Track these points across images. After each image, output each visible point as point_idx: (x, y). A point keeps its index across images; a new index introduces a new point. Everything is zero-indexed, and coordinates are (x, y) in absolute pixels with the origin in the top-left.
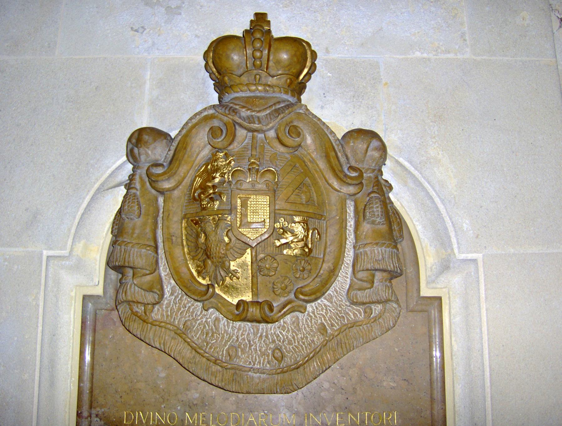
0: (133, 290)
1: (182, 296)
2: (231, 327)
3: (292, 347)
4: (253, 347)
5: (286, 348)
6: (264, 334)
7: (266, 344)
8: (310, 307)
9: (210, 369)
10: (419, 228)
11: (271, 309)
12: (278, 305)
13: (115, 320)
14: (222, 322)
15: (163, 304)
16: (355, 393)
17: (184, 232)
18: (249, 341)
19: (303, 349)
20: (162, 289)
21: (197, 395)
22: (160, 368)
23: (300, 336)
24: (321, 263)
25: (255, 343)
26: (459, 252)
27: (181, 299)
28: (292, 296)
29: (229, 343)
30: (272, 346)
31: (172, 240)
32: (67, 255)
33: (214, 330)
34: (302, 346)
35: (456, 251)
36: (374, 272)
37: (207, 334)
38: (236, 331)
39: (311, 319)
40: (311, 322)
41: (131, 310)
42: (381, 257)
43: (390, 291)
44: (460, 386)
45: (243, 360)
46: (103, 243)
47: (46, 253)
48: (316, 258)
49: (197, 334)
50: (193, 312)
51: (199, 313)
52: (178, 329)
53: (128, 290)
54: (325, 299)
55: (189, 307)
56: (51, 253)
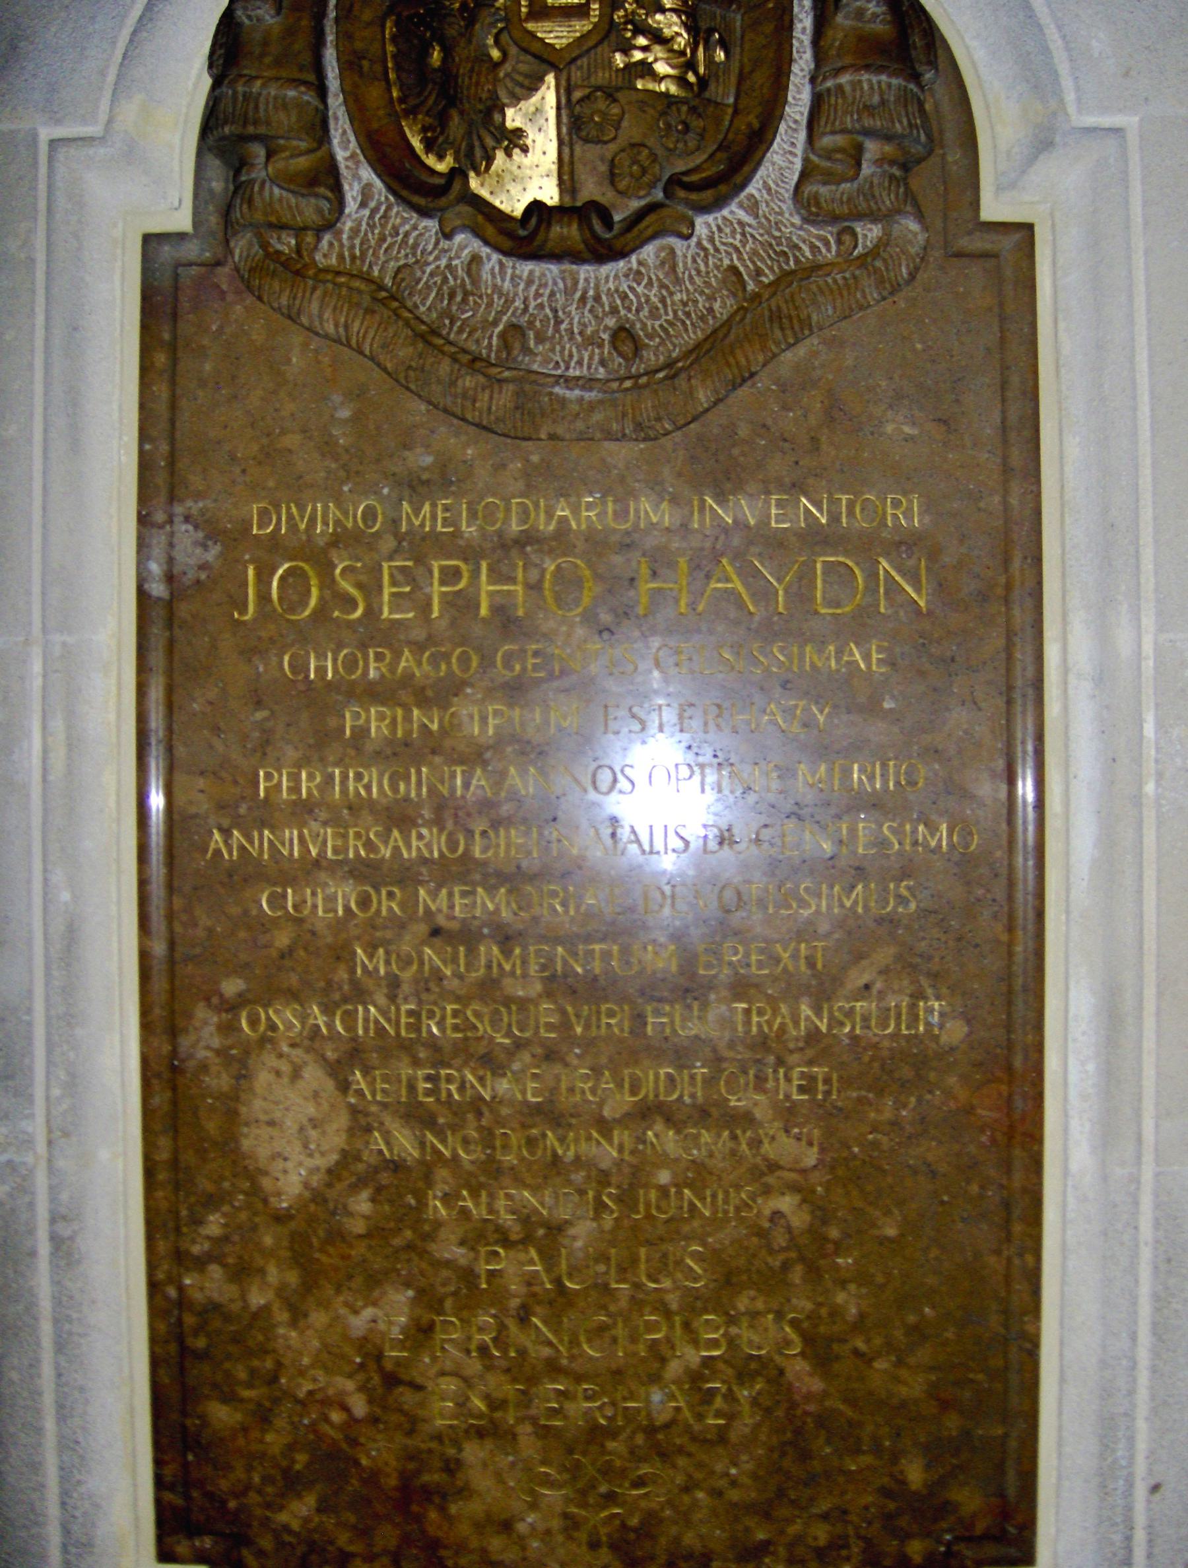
0: (267, 193)
1: (389, 208)
2: (508, 278)
3: (661, 326)
4: (563, 327)
5: (644, 325)
6: (591, 293)
7: (596, 317)
8: (703, 224)
9: (460, 382)
10: (980, 54)
11: (608, 222)
12: (624, 220)
13: (224, 287)
14: (487, 267)
15: (341, 232)
16: (818, 449)
17: (390, 48)
18: (555, 311)
19: (686, 330)
20: (337, 188)
21: (429, 460)
22: (337, 398)
23: (677, 297)
24: (728, 118)
25: (569, 314)
26: (1080, 111)
27: (385, 216)
28: (659, 195)
29: (505, 318)
30: (611, 322)
31: (361, 67)
32: (101, 134)
33: (469, 287)
34: (683, 323)
35: (1072, 109)
36: (860, 138)
37: (452, 296)
38: (522, 286)
39: (706, 256)
40: (707, 265)
41: (265, 245)
42: (876, 99)
43: (902, 190)
44: (1078, 439)
45: (539, 358)
46: (189, 105)
47: (46, 133)
48: (717, 104)
49: (425, 299)
50: (415, 246)
51: (430, 247)
52: (382, 288)
53: (256, 197)
54: (741, 206)
55: (407, 235)
56: (60, 132)
